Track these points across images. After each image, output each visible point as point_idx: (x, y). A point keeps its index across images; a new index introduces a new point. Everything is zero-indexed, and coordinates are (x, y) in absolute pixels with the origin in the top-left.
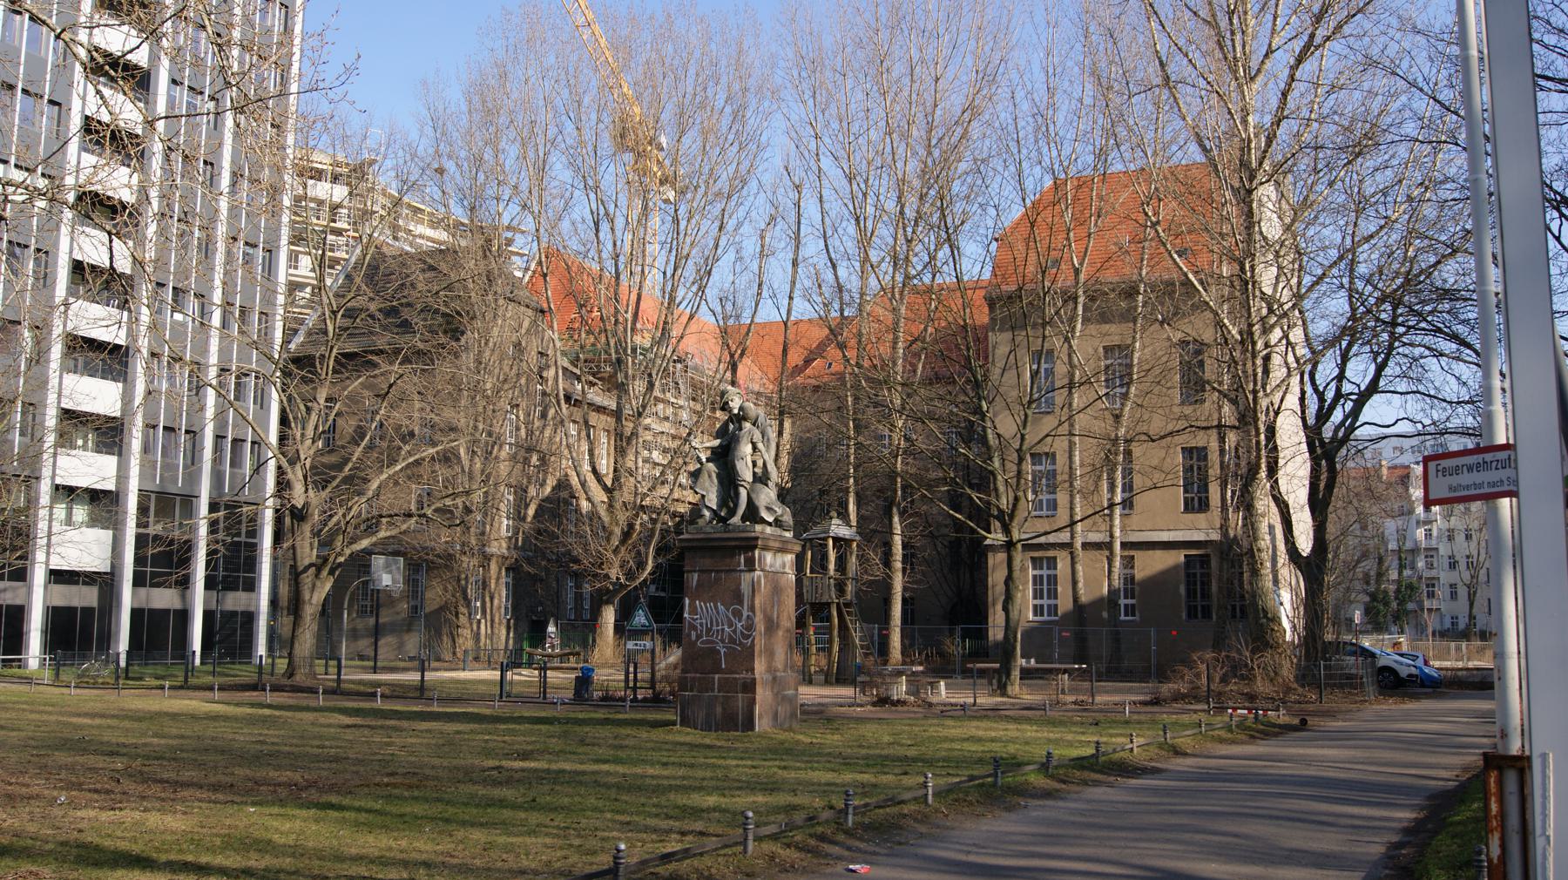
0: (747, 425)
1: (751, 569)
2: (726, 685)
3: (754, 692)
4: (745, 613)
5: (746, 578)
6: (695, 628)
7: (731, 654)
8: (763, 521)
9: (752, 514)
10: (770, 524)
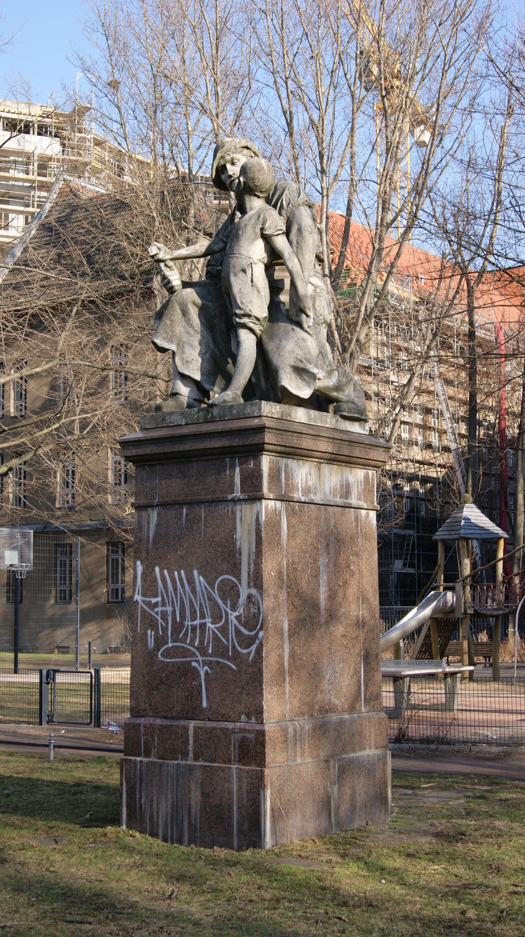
0: (256, 204)
1: (255, 496)
2: (210, 745)
3: (261, 762)
4: (244, 591)
5: (245, 514)
6: (152, 624)
7: (218, 674)
8: (285, 397)
9: (265, 383)
10: (300, 402)
